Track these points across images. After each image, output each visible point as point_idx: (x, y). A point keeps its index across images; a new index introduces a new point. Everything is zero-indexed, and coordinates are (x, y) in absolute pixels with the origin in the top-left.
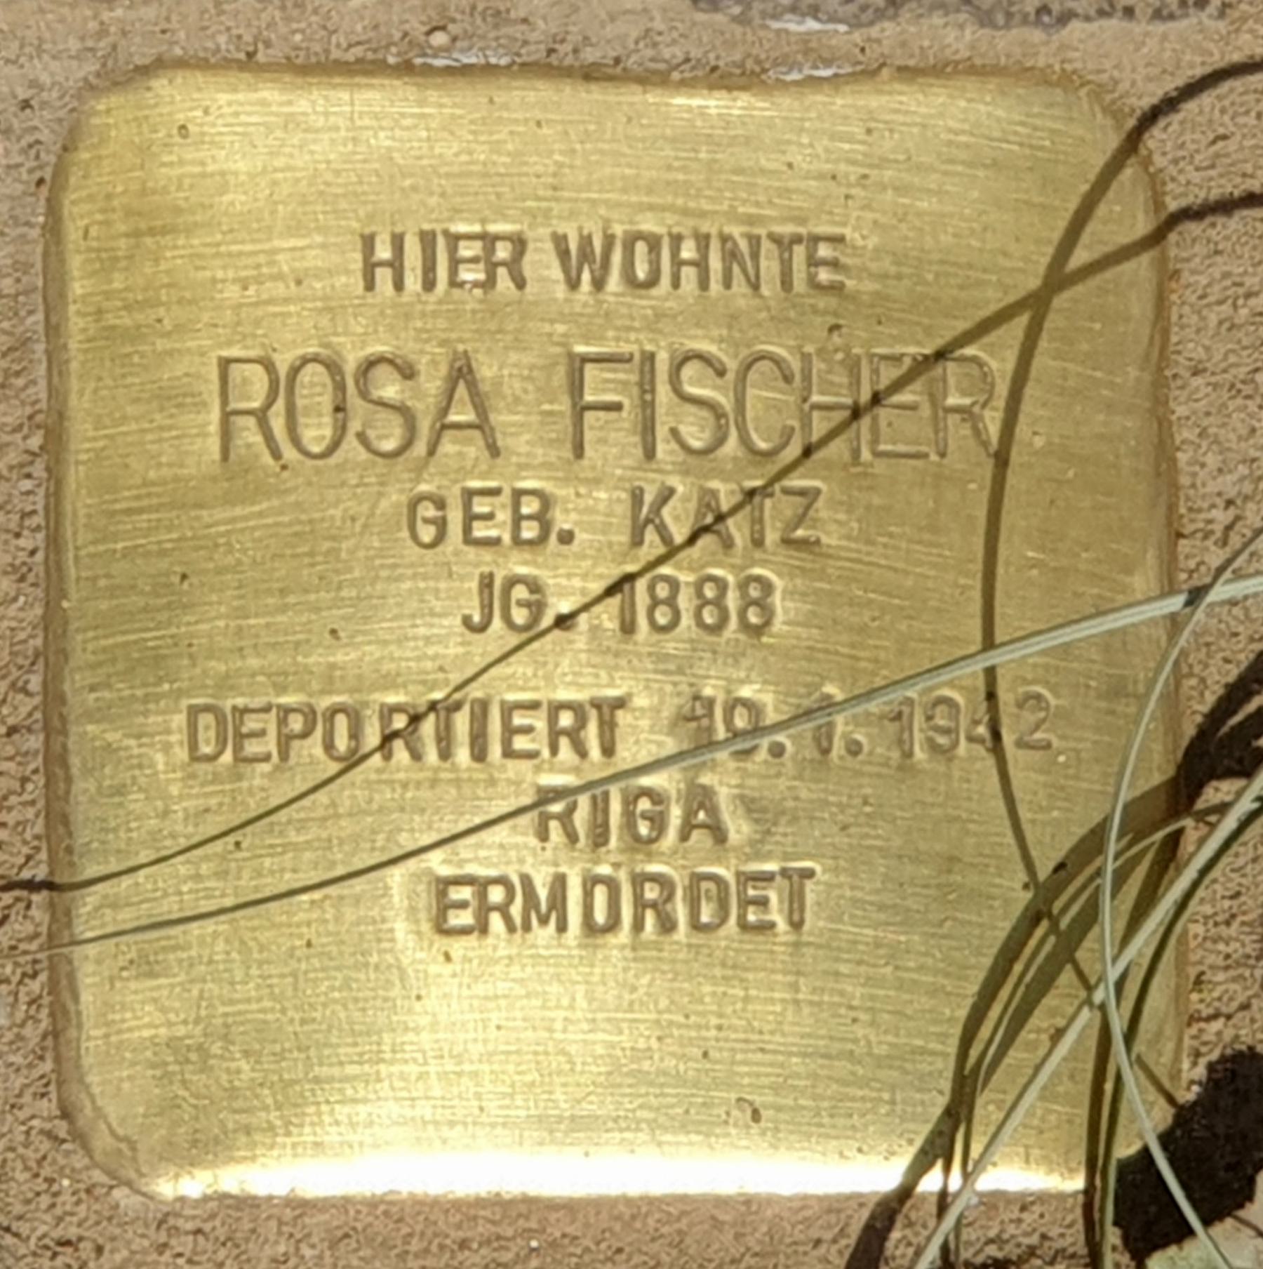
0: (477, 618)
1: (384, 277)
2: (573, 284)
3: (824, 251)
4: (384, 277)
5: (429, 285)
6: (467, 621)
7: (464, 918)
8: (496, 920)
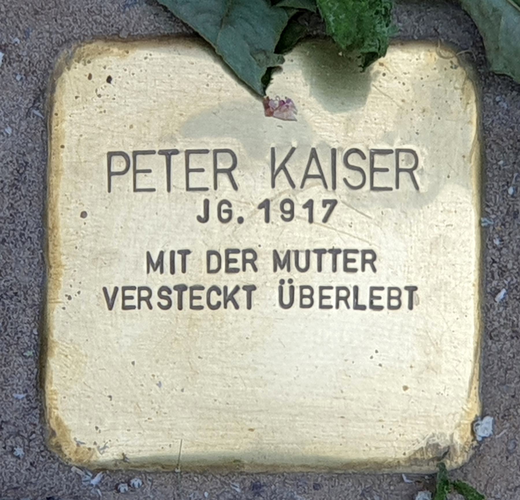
0: (202, 216)
6: (199, 218)
7: (134, 302)
8: (144, 303)
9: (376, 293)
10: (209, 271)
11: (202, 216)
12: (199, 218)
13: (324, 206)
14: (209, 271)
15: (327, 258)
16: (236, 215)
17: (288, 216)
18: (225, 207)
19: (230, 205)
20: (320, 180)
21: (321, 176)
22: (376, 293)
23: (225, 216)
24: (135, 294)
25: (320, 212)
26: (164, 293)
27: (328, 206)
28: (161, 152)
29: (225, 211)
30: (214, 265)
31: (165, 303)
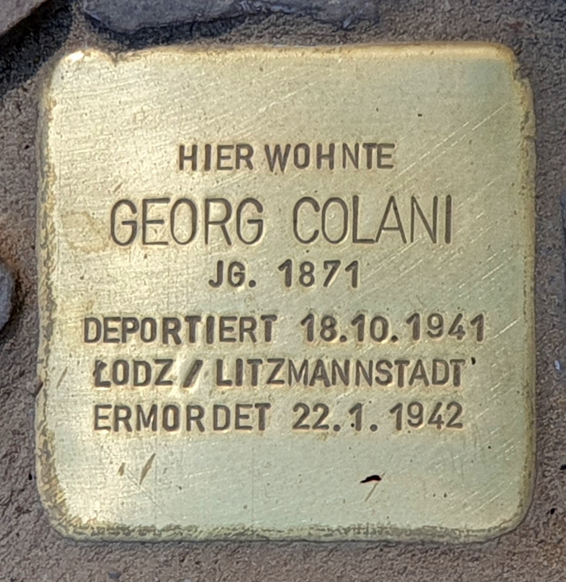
0: (215, 280)
1: (188, 164)
2: (272, 168)
3: (385, 151)
4: (188, 164)
5: (369, 165)
6: (211, 282)
7: (108, 423)
9: (101, 412)
10: (87, 340)
11: (215, 280)
12: (211, 282)
13: (326, 267)
14: (87, 340)
15: (200, 328)
16: (248, 277)
17: (415, 421)
18: (236, 269)
19: (242, 267)
20: (398, 232)
21: (400, 228)
22: (101, 412)
23: (235, 280)
24: (109, 412)
25: (320, 274)
26: (384, 366)
27: (330, 267)
28: (257, 405)
29: (236, 274)
30: (92, 335)
31: (384, 378)
